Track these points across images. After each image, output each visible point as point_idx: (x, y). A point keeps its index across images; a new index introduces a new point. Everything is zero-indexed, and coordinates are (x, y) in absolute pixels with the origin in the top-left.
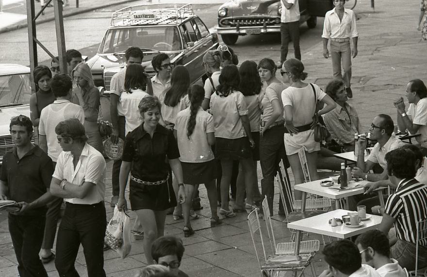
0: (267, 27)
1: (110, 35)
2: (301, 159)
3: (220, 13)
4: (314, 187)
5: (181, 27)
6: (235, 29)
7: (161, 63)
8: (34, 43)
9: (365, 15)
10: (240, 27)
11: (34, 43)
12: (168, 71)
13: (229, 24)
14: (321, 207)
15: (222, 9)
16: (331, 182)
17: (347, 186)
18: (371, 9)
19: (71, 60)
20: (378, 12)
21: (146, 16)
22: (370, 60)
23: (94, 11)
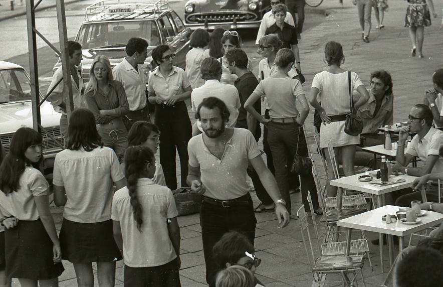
0: (238, 23)
1: (84, 30)
2: (330, 152)
3: (187, 9)
4: (351, 181)
5: (159, 22)
6: (203, 25)
7: (162, 55)
8: (33, 33)
9: (333, 11)
10: (209, 24)
11: (33, 33)
12: (170, 62)
13: (197, 21)
14: (352, 204)
15: (189, 5)
16: (369, 176)
17: (387, 181)
18: (340, 5)
19: (74, 52)
20: (346, 8)
21: (122, 10)
22: (351, 55)
23: (46, 10)
